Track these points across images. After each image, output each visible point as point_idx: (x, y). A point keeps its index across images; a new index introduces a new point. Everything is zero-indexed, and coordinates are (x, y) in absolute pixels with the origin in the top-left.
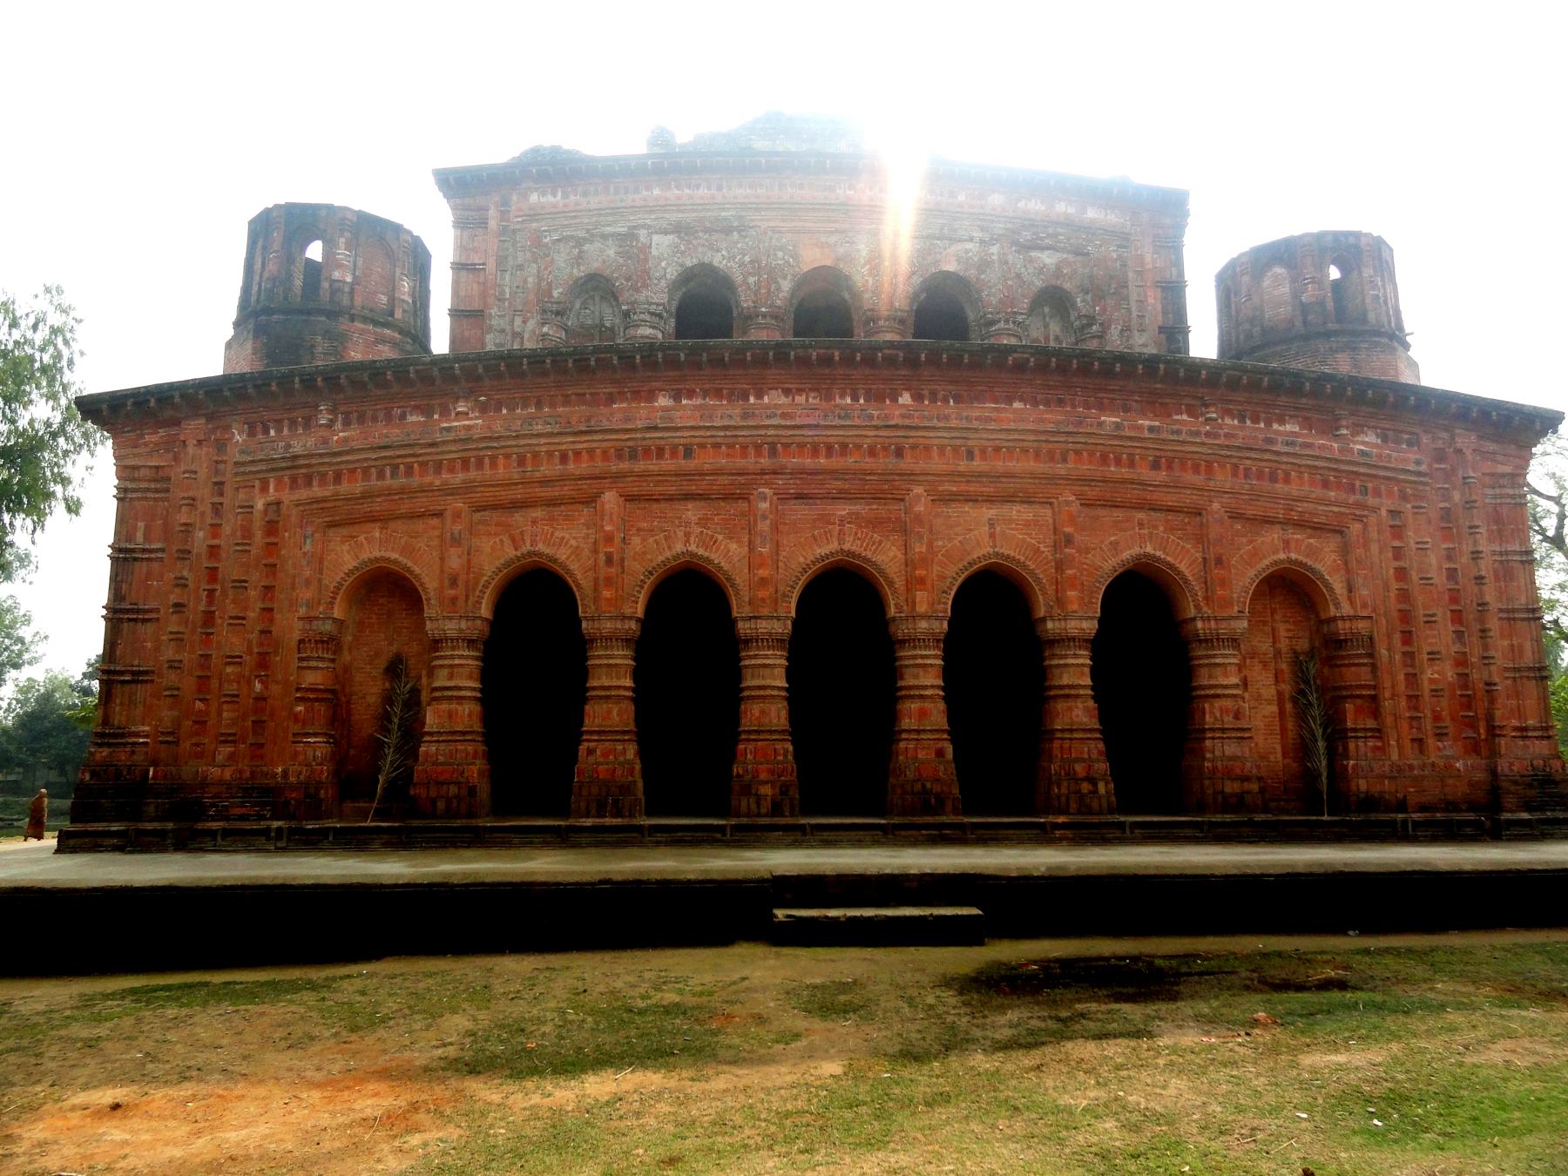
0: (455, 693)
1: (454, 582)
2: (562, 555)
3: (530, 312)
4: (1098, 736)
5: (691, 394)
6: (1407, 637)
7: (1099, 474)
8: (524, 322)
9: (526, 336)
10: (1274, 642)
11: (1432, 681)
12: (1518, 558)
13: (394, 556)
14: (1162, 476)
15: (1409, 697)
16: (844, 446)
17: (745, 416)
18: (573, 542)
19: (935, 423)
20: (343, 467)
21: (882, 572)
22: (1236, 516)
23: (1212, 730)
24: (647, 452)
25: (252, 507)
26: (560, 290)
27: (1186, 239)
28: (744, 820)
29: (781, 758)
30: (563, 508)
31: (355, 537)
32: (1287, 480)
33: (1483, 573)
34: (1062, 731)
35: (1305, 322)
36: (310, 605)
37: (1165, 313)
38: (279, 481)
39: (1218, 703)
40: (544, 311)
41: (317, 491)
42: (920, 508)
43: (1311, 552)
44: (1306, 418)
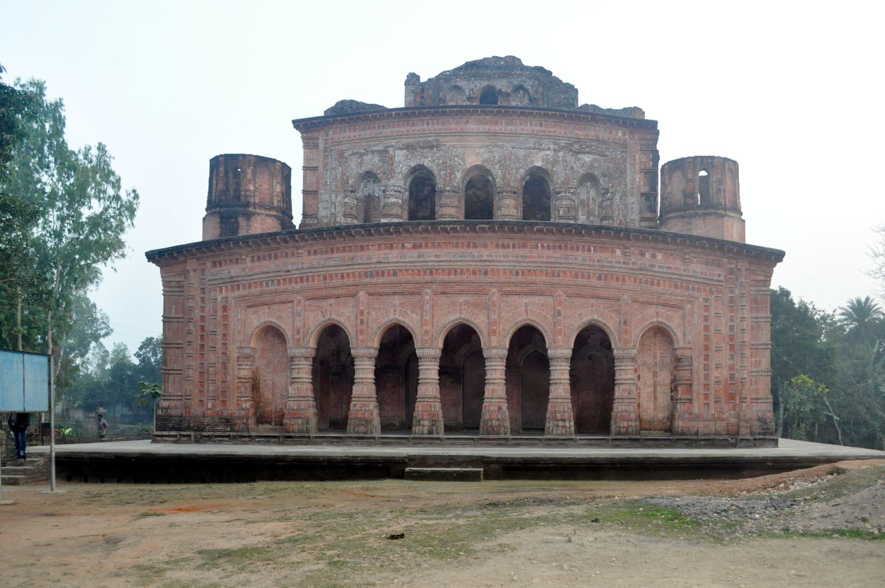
9: (337, 204)
11: (716, 377)
12: (763, 320)
13: (274, 320)
16: (462, 270)
17: (419, 256)
18: (347, 314)
22: (635, 301)
24: (377, 273)
32: (658, 284)
39: (622, 387)
41: (241, 292)
42: (495, 298)
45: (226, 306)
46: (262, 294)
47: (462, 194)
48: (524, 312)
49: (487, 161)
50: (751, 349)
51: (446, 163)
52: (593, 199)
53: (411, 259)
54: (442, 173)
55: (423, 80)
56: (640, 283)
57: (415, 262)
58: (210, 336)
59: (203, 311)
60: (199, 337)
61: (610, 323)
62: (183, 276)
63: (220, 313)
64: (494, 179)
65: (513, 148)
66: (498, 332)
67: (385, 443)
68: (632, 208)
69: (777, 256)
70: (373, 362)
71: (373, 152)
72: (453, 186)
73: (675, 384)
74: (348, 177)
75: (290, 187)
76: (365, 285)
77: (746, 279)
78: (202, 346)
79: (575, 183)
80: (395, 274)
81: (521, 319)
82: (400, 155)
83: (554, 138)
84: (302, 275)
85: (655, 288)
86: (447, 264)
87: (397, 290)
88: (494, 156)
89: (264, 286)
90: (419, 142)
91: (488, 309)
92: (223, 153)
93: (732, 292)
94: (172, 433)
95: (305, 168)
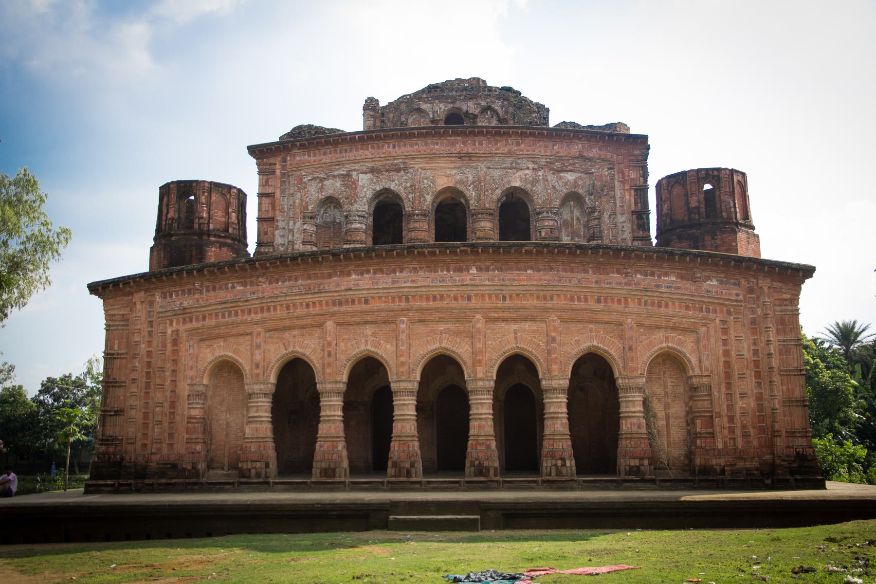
0: (259, 419)
2: (307, 352)
7: (569, 306)
9: (295, 231)
11: (741, 408)
13: (230, 354)
14: (601, 306)
17: (394, 282)
18: (313, 346)
22: (640, 325)
24: (347, 302)
26: (312, 206)
30: (307, 329)
32: (667, 306)
39: (629, 420)
40: (304, 217)
41: (195, 324)
42: (479, 325)
43: (681, 343)
45: (177, 340)
46: (217, 326)
47: (432, 217)
48: (513, 339)
49: (461, 182)
50: (781, 375)
51: (415, 186)
53: (384, 286)
54: (411, 196)
55: (383, 103)
56: (645, 305)
57: (389, 288)
58: (157, 373)
59: (150, 346)
60: (145, 374)
61: (611, 348)
62: (129, 309)
63: (169, 347)
64: (467, 201)
65: (488, 168)
66: (483, 362)
67: (355, 487)
68: (623, 227)
69: (808, 271)
70: (341, 399)
71: (334, 177)
73: (691, 416)
74: (307, 203)
75: (245, 214)
76: (333, 314)
77: (769, 298)
78: (148, 385)
79: (557, 203)
80: (367, 302)
81: (510, 347)
82: (364, 179)
83: (534, 159)
84: (263, 305)
85: (663, 310)
87: (369, 319)
88: (467, 178)
89: (220, 317)
90: (385, 164)
91: (472, 337)
92: (175, 180)
93: (753, 313)
94: (109, 482)
95: (260, 195)
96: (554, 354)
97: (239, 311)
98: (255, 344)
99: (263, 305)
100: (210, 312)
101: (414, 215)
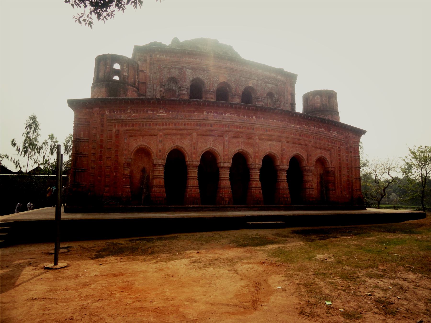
0: (160, 177)
1: (160, 151)
2: (184, 146)
3: (158, 84)
4: (198, 188)
5: (211, 112)
6: (340, 172)
8: (156, 87)
9: (157, 90)
10: (317, 172)
11: (344, 180)
13: (146, 144)
14: (301, 138)
15: (340, 183)
16: (243, 127)
17: (223, 118)
18: (186, 144)
19: (260, 123)
20: (134, 123)
21: (249, 154)
22: (313, 147)
23: (254, 187)
24: (203, 125)
25: (112, 131)
26: (165, 80)
27: (296, 85)
28: (223, 206)
29: (229, 193)
30: (184, 136)
31: (136, 139)
32: (322, 140)
33: (352, 160)
34: (282, 188)
35: (323, 108)
36: (126, 155)
37: (291, 100)
38: (118, 126)
39: (309, 183)
40: (161, 85)
41: (128, 128)
42: (257, 141)
44: (325, 128)
45: (118, 135)
52: (270, 103)
53: (219, 120)
69: (363, 132)
72: (213, 90)
80: (211, 126)
84: (163, 122)
86: (236, 123)
89: (168, 125)
96: (284, 155)
97: (151, 124)
98: (159, 140)
99: (163, 122)
100: (136, 123)
101: (210, 91)
